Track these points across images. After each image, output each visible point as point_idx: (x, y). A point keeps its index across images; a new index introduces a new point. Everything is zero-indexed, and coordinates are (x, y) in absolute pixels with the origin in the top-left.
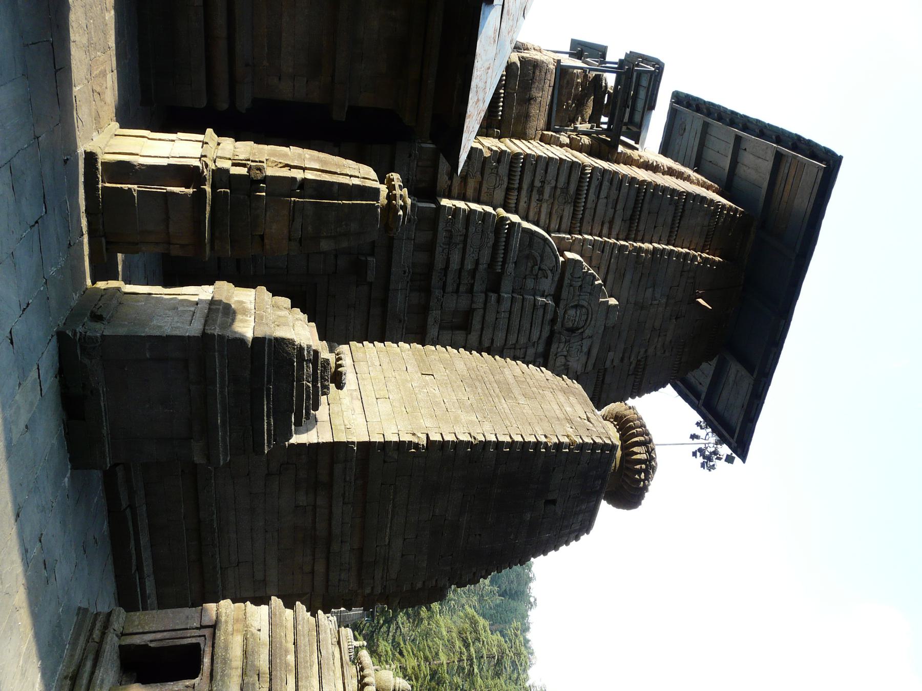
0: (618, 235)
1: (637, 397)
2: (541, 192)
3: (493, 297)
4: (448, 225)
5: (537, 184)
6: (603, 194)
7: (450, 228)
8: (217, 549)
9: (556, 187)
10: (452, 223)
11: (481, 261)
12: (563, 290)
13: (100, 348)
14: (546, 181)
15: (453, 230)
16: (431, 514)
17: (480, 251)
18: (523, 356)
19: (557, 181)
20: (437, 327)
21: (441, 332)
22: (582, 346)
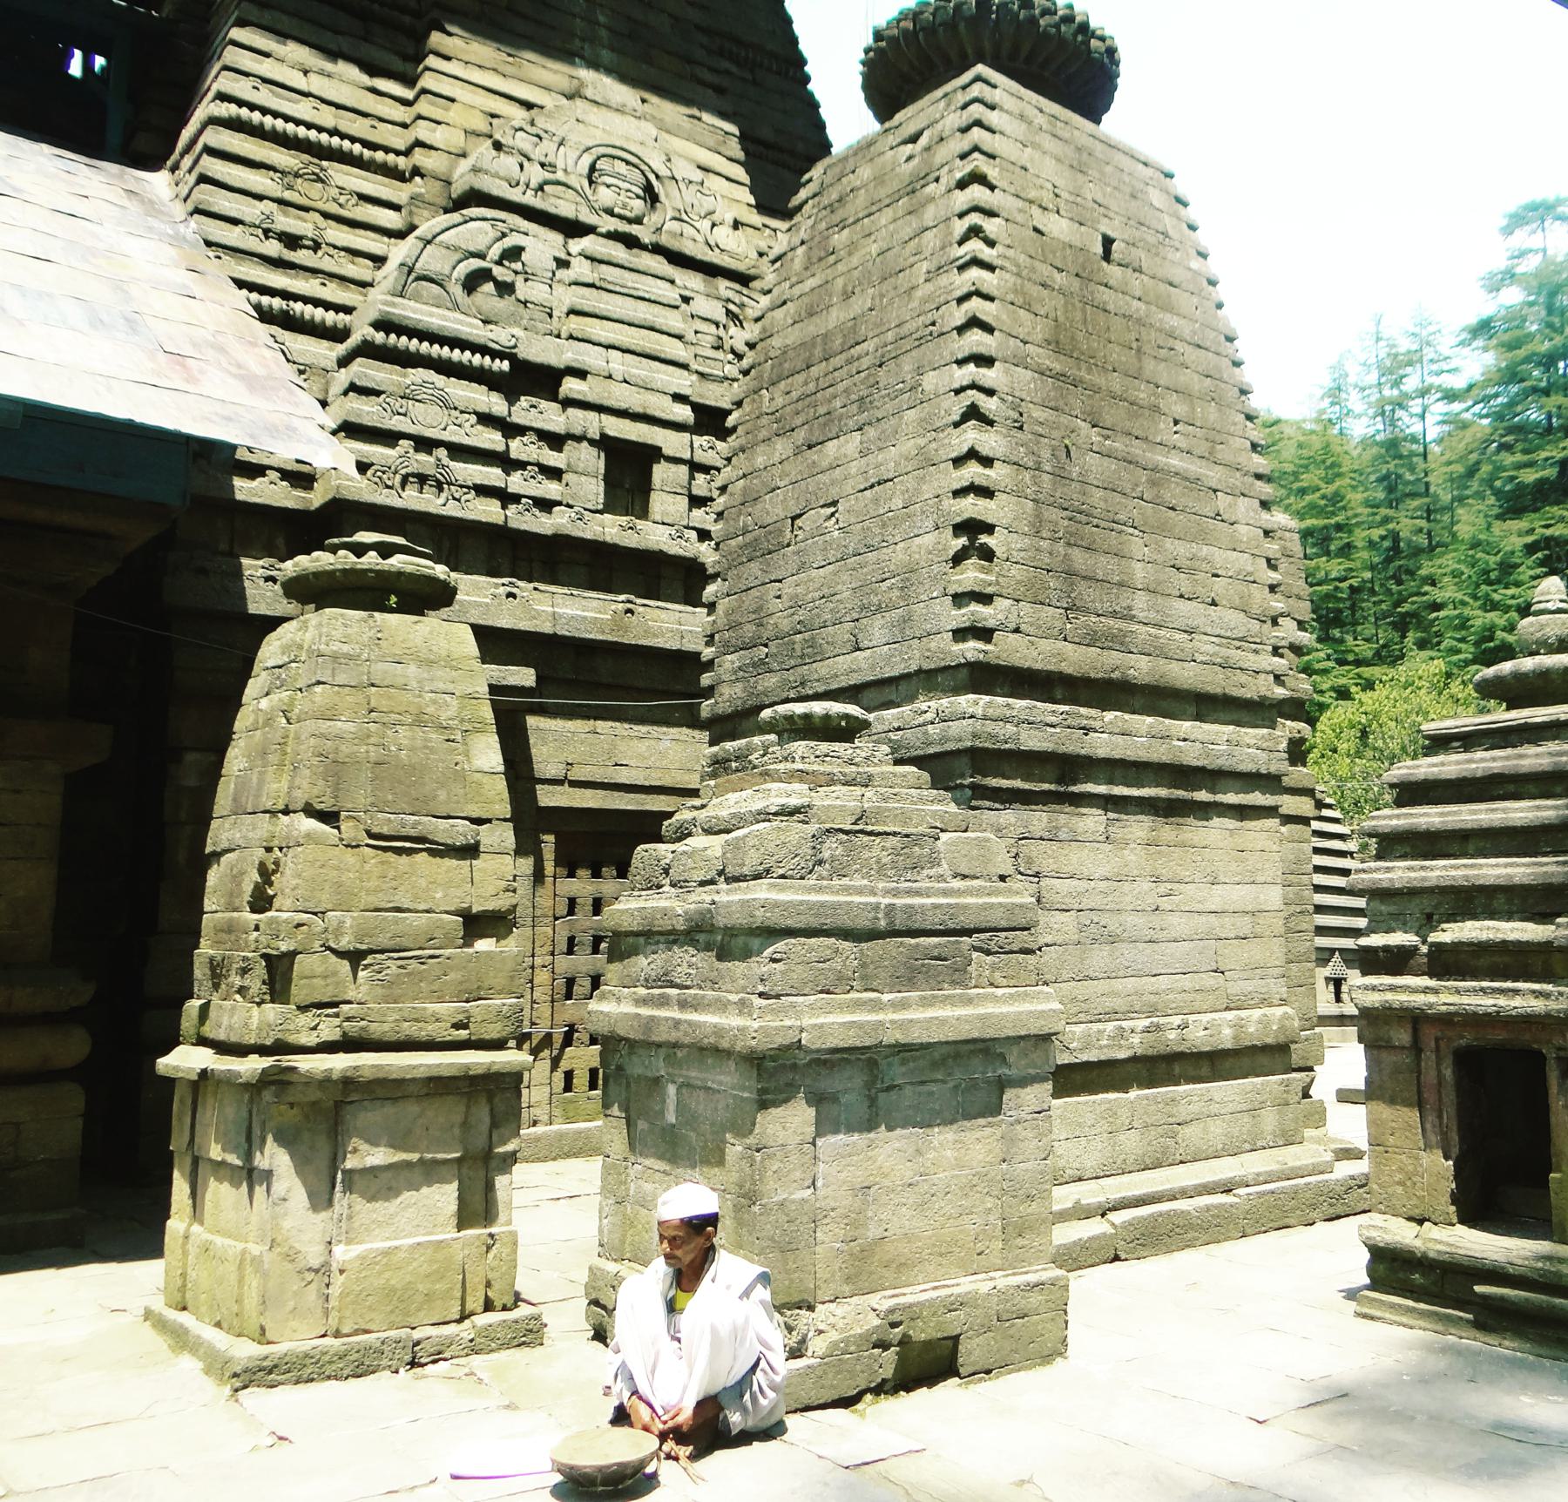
0: (405, 58)
1: (806, 68)
2: (292, 241)
3: (570, 386)
4: (389, 483)
5: (273, 248)
6: (298, 81)
7: (398, 478)
8: (1191, 1018)
9: (281, 202)
10: (384, 473)
11: (483, 409)
12: (552, 210)
13: (789, 1313)
14: (264, 226)
15: (403, 472)
16: (1131, 530)
17: (456, 409)
18: (714, 327)
19: (260, 197)
20: (640, 524)
21: (658, 518)
22: (690, 182)
